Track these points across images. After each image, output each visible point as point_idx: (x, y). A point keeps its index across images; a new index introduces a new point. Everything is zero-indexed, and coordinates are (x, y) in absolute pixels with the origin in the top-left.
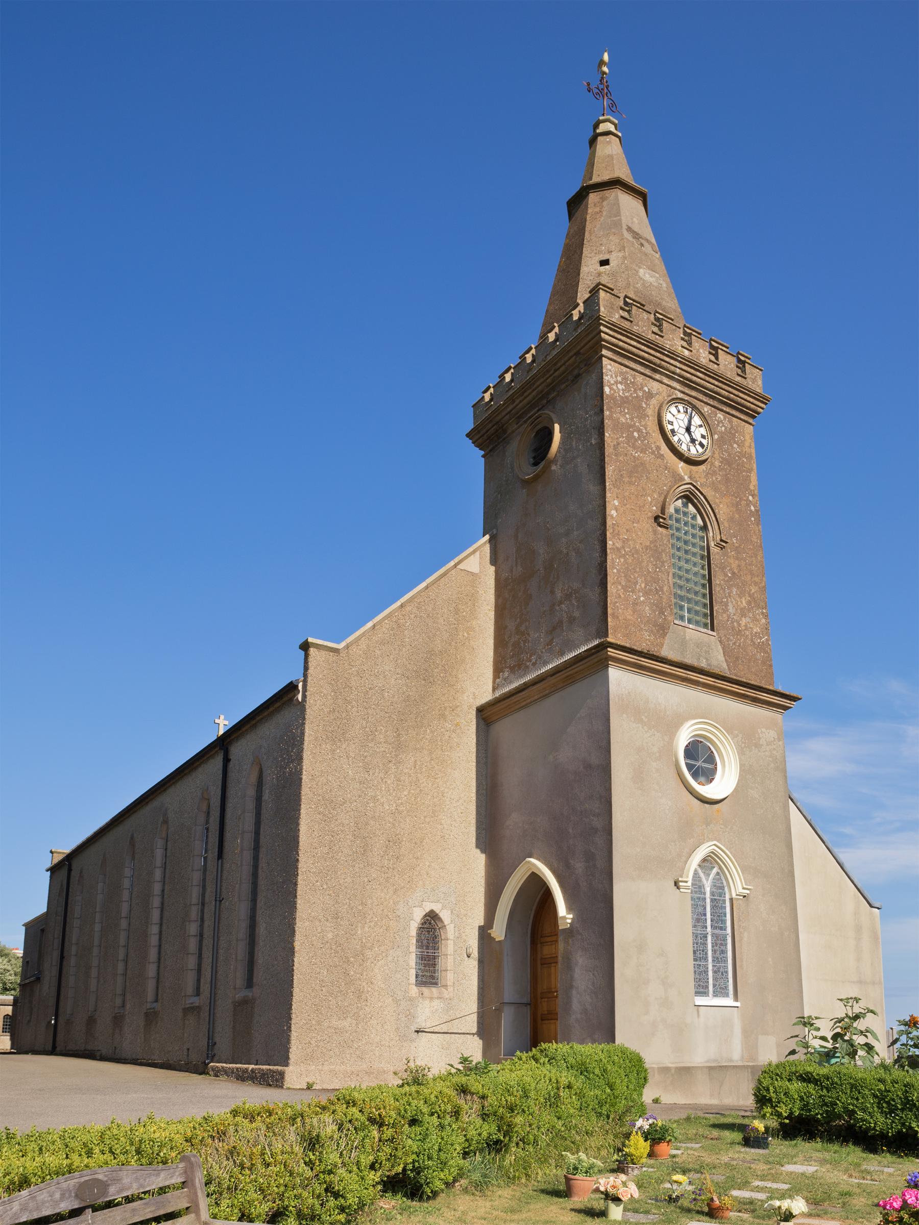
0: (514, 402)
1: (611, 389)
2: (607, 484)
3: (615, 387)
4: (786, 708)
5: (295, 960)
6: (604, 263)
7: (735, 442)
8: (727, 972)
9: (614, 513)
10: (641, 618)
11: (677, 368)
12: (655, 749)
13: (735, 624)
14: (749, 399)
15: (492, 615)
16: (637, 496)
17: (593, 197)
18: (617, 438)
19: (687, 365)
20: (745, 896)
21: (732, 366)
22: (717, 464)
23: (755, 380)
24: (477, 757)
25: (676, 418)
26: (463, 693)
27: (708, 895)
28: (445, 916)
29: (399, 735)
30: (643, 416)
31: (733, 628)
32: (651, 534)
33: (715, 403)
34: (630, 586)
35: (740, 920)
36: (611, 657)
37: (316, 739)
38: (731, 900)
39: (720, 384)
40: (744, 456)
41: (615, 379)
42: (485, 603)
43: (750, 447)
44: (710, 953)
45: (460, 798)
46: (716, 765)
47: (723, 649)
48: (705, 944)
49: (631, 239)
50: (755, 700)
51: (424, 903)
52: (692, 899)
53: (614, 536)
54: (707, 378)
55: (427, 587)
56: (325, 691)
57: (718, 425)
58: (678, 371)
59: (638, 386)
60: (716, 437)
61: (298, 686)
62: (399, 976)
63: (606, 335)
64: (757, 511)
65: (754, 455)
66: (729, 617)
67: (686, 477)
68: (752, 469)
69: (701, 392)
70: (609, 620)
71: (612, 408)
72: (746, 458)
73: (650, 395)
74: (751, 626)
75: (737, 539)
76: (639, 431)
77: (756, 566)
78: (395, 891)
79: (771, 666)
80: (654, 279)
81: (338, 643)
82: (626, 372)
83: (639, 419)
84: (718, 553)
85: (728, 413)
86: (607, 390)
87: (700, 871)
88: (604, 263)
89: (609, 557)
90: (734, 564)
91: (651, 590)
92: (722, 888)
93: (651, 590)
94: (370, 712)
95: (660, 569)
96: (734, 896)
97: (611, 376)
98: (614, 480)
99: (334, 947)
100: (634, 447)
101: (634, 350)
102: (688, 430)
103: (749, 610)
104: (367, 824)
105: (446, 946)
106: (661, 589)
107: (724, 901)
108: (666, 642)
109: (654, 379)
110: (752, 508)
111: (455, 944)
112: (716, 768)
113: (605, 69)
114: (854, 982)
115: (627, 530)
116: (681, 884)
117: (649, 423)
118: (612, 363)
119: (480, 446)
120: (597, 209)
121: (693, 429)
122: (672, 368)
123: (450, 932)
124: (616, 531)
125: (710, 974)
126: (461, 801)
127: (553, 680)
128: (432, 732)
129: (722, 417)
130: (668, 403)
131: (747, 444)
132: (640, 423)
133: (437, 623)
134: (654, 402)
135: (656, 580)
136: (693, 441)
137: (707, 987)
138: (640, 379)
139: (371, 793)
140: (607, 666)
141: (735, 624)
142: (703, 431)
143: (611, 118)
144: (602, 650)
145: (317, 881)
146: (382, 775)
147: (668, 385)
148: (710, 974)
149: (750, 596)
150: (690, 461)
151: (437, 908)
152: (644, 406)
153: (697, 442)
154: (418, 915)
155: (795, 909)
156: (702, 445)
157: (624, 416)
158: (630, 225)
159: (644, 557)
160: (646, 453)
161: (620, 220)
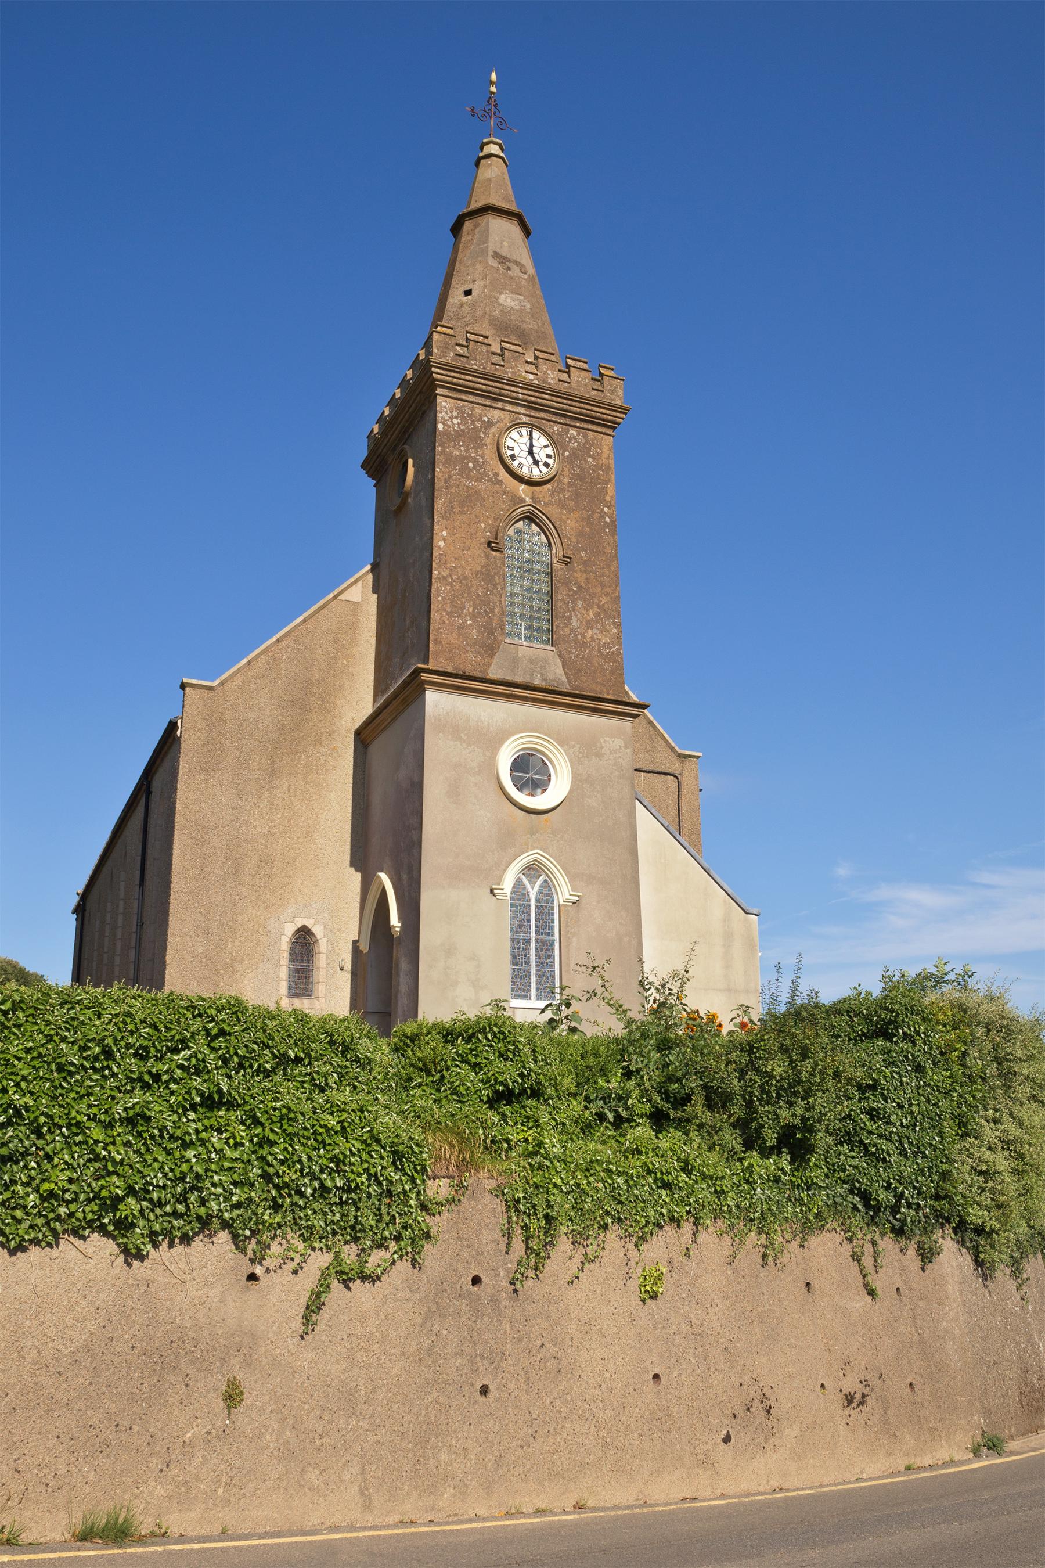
0: (387, 435)
1: (444, 425)
2: (436, 517)
3: (449, 423)
4: (635, 716)
5: (167, 972)
6: (468, 293)
7: (590, 456)
8: (553, 977)
9: (442, 544)
10: (466, 641)
11: (520, 393)
12: (474, 765)
13: (579, 637)
14: (604, 411)
15: (373, 641)
16: (469, 525)
17: (468, 225)
18: (449, 472)
19: (530, 390)
20: (574, 903)
21: (587, 381)
22: (566, 480)
23: (616, 393)
24: (354, 778)
25: (516, 442)
26: (341, 718)
27: (533, 902)
28: (318, 931)
29: (273, 762)
30: (479, 444)
31: (576, 641)
32: (483, 560)
33: (568, 421)
34: (457, 611)
35: (567, 926)
36: (425, 681)
37: (190, 770)
38: (559, 905)
39: (569, 402)
40: (601, 468)
41: (450, 415)
42: (366, 630)
43: (608, 458)
44: (533, 958)
45: (336, 818)
46: (550, 776)
47: (563, 662)
48: (528, 949)
49: (496, 265)
50: (595, 711)
51: (296, 919)
52: (512, 905)
53: (440, 566)
54: (554, 399)
55: (305, 621)
56: (199, 726)
57: (569, 442)
58: (521, 396)
59: (476, 417)
60: (567, 454)
61: (176, 723)
62: (269, 988)
63: (438, 374)
64: (613, 522)
65: (612, 466)
66: (571, 630)
67: (527, 499)
68: (609, 480)
69: (549, 412)
70: (431, 645)
71: (444, 443)
72: (603, 470)
73: (490, 424)
74: (599, 637)
75: (586, 553)
76: (475, 461)
77: (609, 577)
78: (266, 908)
79: (622, 675)
80: (516, 303)
81: (213, 681)
82: (464, 406)
83: (476, 450)
84: (562, 569)
85: (583, 428)
86: (440, 426)
87: (524, 878)
88: (468, 293)
89: (434, 587)
90: (581, 578)
91: (479, 613)
92: (550, 895)
93: (479, 613)
94: (244, 742)
95: (491, 591)
96: (561, 902)
97: (446, 413)
98: (443, 512)
99: (204, 960)
100: (468, 477)
101: (470, 384)
102: (531, 453)
103: (597, 622)
104: (239, 846)
105: (319, 959)
106: (492, 611)
107: (553, 908)
108: (494, 661)
109: (495, 408)
110: (607, 519)
111: (327, 957)
112: (550, 780)
113: (493, 89)
114: (720, 990)
115: (456, 559)
116: (495, 891)
117: (487, 452)
118: (448, 400)
119: (371, 475)
120: (469, 238)
121: (535, 450)
122: (514, 395)
123: (323, 946)
124: (443, 561)
125: (533, 978)
126: (336, 821)
127: (395, 703)
128: (308, 757)
129: (575, 433)
130: (506, 431)
131: (605, 456)
132: (476, 453)
133: (315, 654)
134: (494, 429)
135: (486, 603)
136: (536, 462)
137: (529, 991)
138: (478, 410)
139: (244, 817)
140: (424, 690)
141: (579, 637)
142: (549, 451)
143: (495, 140)
144: (416, 677)
145: (189, 900)
146: (255, 800)
147: (511, 411)
148: (533, 978)
149: (599, 607)
150: (530, 483)
151: (308, 924)
152: (482, 435)
153: (541, 464)
154: (290, 930)
155: (639, 915)
156: (546, 465)
157: (459, 448)
158: (498, 250)
159: (474, 582)
160: (481, 482)
161: (487, 247)
